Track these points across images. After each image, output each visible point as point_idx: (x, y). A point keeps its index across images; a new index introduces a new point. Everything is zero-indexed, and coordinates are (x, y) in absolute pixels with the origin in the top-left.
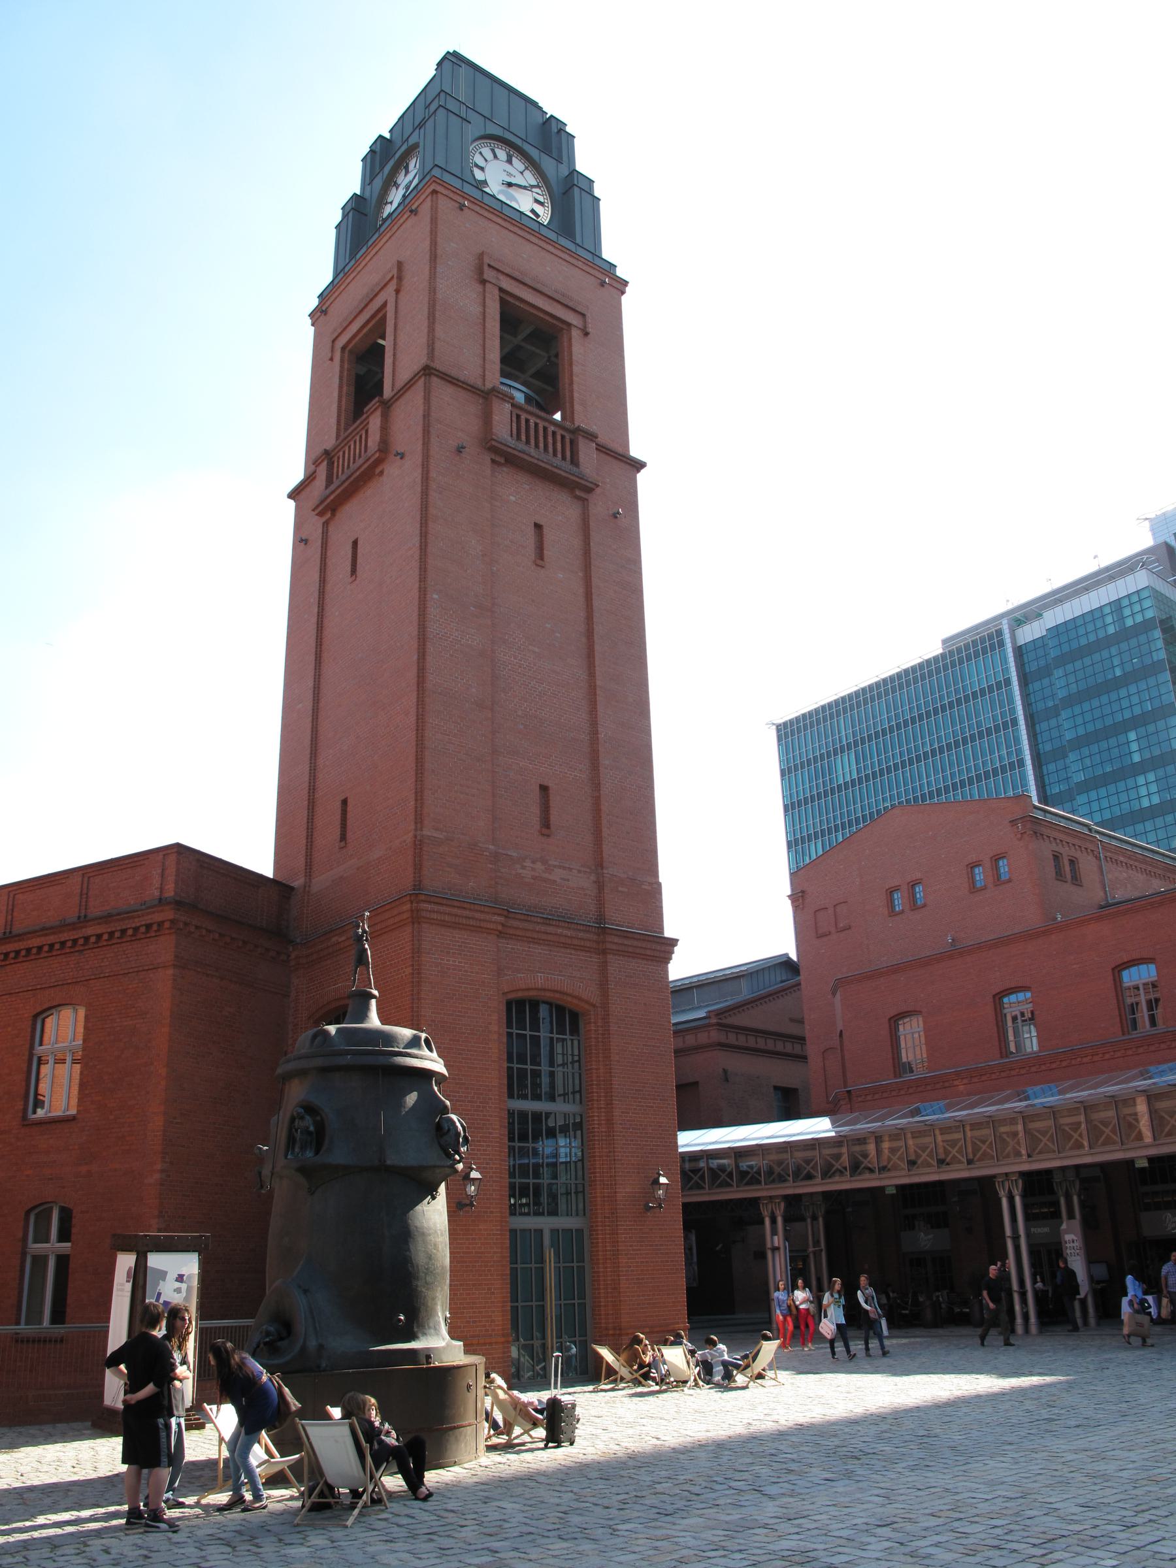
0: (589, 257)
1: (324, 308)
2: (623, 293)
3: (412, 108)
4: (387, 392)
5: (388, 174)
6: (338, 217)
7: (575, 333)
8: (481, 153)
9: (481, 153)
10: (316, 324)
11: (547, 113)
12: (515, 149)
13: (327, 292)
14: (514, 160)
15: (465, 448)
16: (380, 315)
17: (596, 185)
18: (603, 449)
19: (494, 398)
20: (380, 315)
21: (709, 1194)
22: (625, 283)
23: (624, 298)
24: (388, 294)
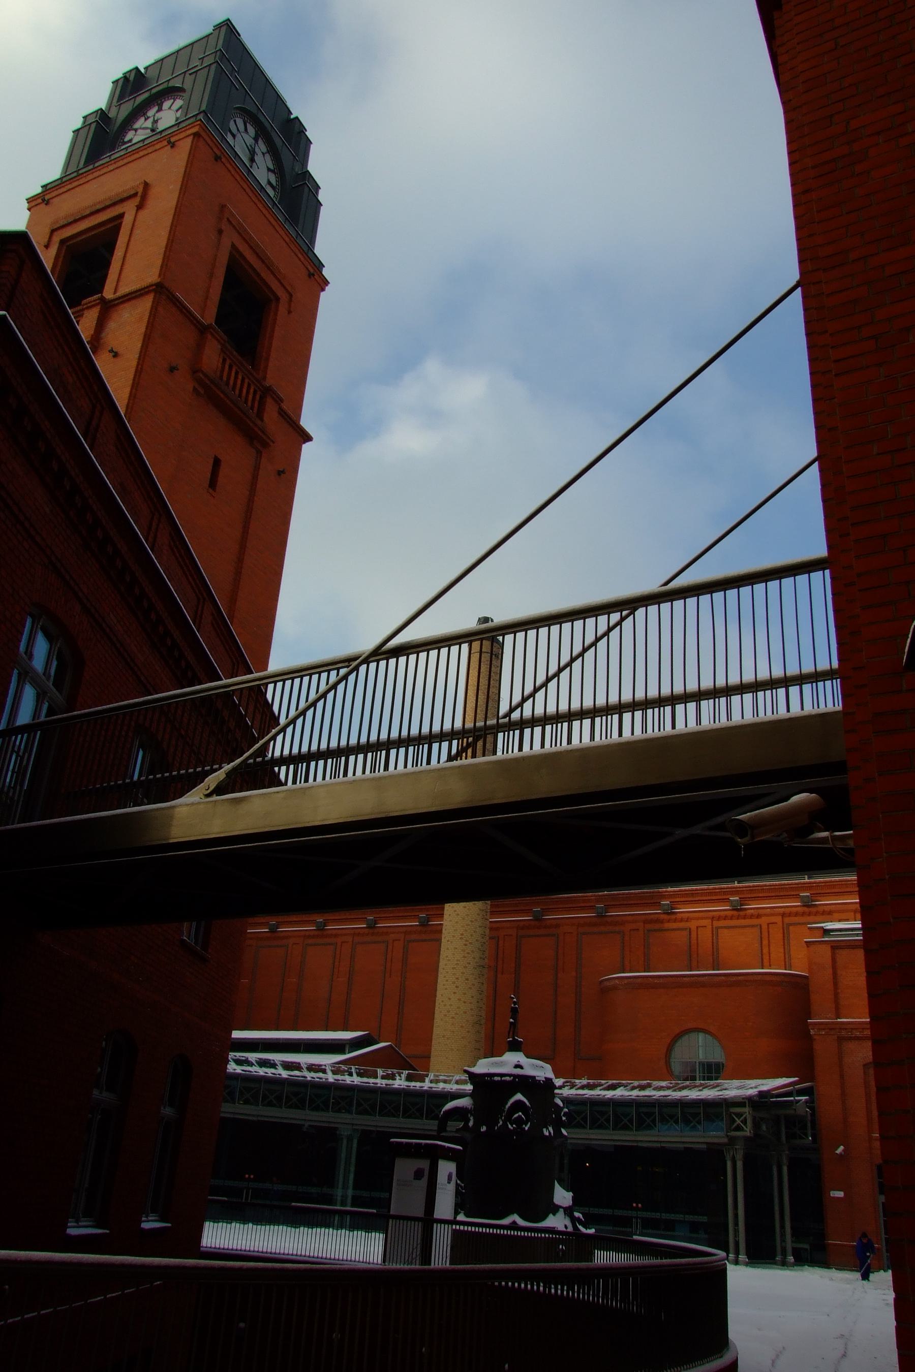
0: (306, 249)
1: (47, 198)
2: (323, 290)
3: (159, 64)
4: (108, 293)
5: (139, 105)
6: (78, 124)
7: (282, 309)
8: (235, 121)
9: (235, 121)
10: (32, 209)
11: (292, 114)
12: (262, 133)
13: (53, 185)
14: (260, 142)
15: (178, 370)
16: (116, 223)
17: (320, 191)
18: (283, 414)
19: (209, 336)
20: (116, 223)
21: (635, 1135)
22: (326, 283)
23: (322, 294)
24: (129, 209)
